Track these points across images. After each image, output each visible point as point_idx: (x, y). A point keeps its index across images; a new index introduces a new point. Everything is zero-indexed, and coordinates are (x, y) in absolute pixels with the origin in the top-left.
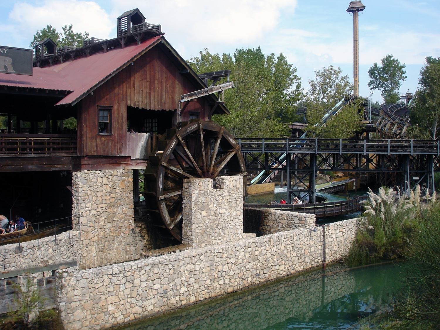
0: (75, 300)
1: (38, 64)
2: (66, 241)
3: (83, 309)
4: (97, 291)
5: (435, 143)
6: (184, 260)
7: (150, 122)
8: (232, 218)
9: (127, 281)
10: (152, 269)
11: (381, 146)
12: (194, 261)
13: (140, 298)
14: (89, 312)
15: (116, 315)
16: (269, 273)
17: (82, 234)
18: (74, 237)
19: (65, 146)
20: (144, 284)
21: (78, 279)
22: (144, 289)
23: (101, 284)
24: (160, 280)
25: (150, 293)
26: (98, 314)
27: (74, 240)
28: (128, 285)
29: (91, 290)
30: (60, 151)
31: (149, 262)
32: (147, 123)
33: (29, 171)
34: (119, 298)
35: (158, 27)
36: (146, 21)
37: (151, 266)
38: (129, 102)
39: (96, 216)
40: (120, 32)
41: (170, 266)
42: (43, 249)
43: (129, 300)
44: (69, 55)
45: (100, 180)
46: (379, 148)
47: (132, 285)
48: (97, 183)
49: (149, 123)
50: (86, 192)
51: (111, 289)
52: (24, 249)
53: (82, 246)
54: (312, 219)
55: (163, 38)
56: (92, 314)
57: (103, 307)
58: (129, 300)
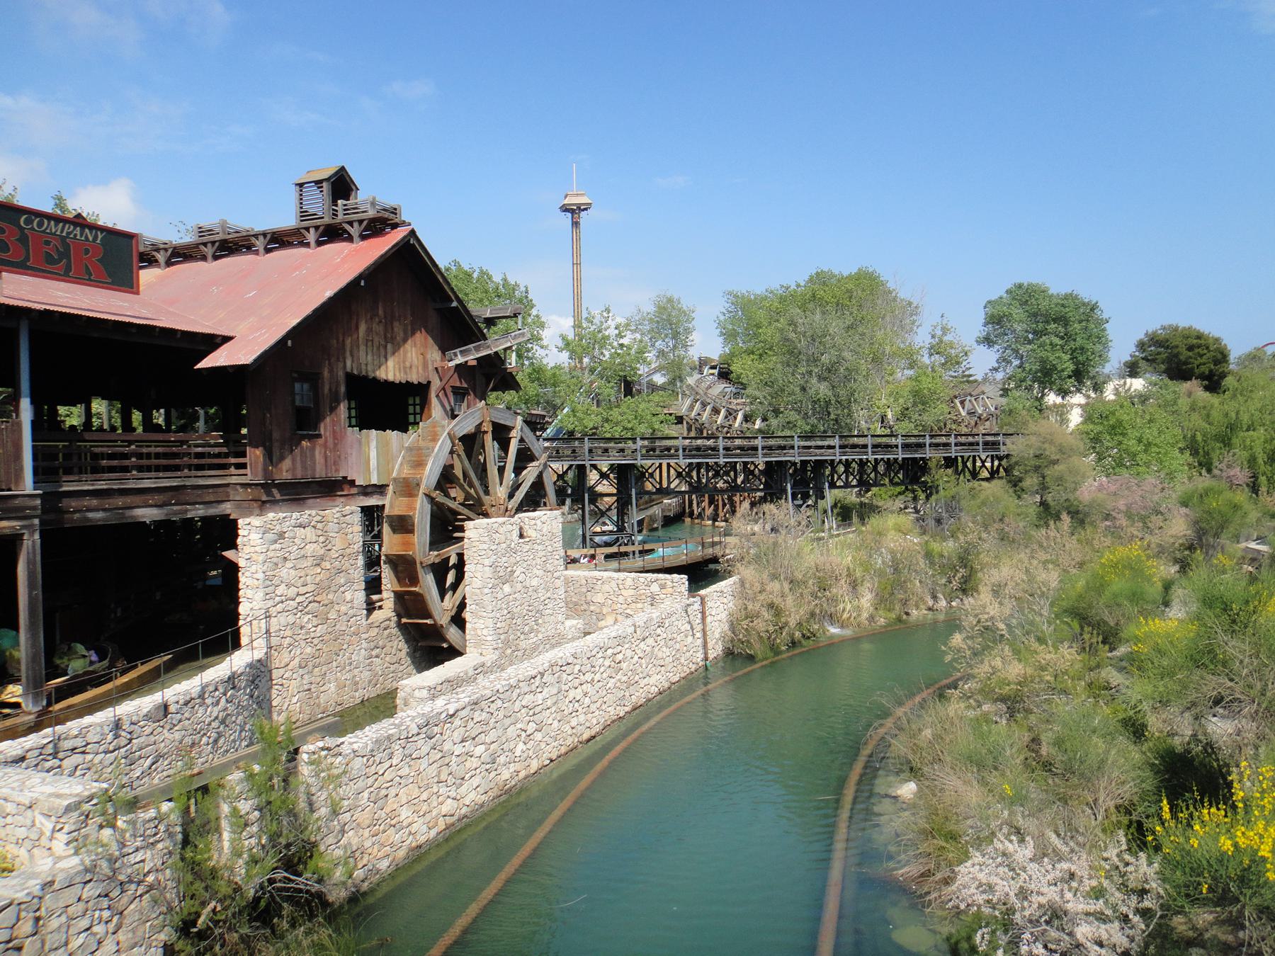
5: (577, 442)
11: (668, 449)
12: (533, 687)
15: (414, 828)
16: (637, 694)
19: (196, 461)
30: (153, 474)
33: (129, 521)
38: (349, 363)
46: (133, 459)
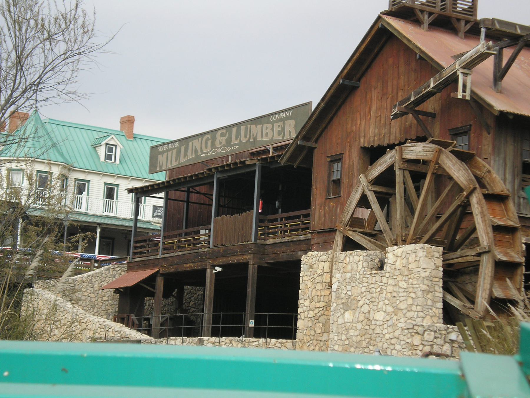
8: (397, 333)
38: (362, 140)
54: (417, 333)
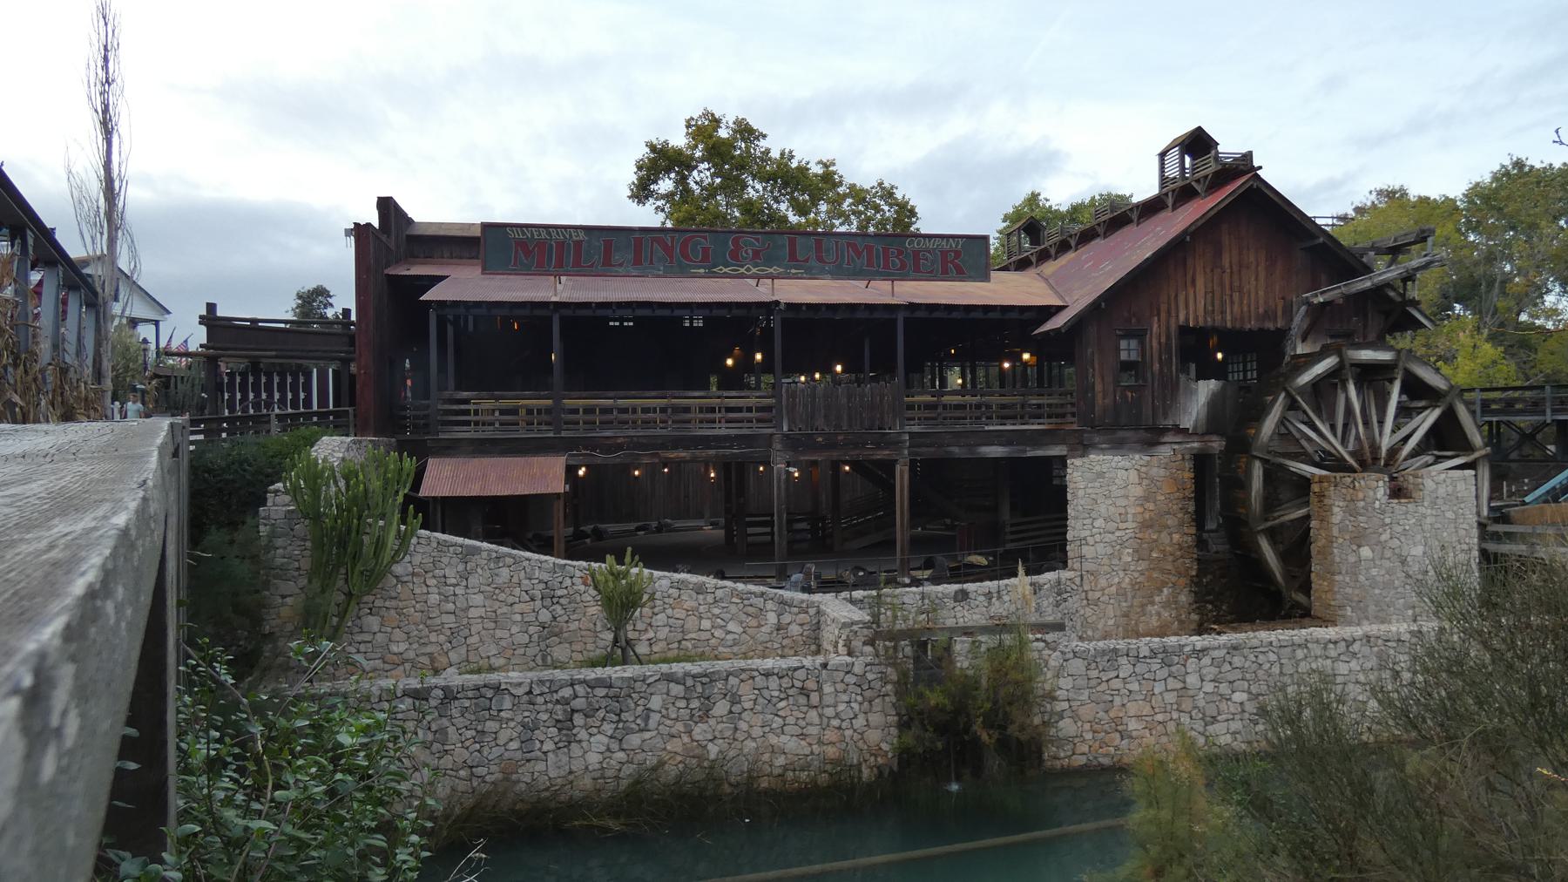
0: (1061, 698)
1: (1012, 267)
2: (1052, 587)
3: (1076, 717)
4: (1104, 686)
6: (1307, 648)
7: (1241, 359)
9: (1169, 675)
10: (1228, 658)
13: (1201, 715)
14: (1087, 726)
17: (1085, 577)
18: (1068, 583)
20: (1209, 687)
21: (1067, 656)
22: (1209, 698)
23: (1113, 674)
24: (1246, 683)
25: (1223, 706)
26: (1107, 733)
27: (1069, 589)
28: (1172, 683)
29: (1093, 682)
31: (1222, 642)
32: (1233, 372)
34: (1153, 708)
35: (1248, 156)
36: (1220, 149)
37: (1226, 651)
39: (1114, 544)
40: (1164, 180)
41: (1273, 657)
42: (1006, 598)
43: (1175, 716)
44: (1068, 242)
45: (1121, 473)
47: (1181, 685)
48: (1117, 481)
49: (1238, 363)
50: (1094, 496)
51: (1135, 686)
52: (971, 596)
53: (1085, 602)
55: (1258, 177)
56: (1094, 732)
57: (1117, 721)
58: (1175, 716)
